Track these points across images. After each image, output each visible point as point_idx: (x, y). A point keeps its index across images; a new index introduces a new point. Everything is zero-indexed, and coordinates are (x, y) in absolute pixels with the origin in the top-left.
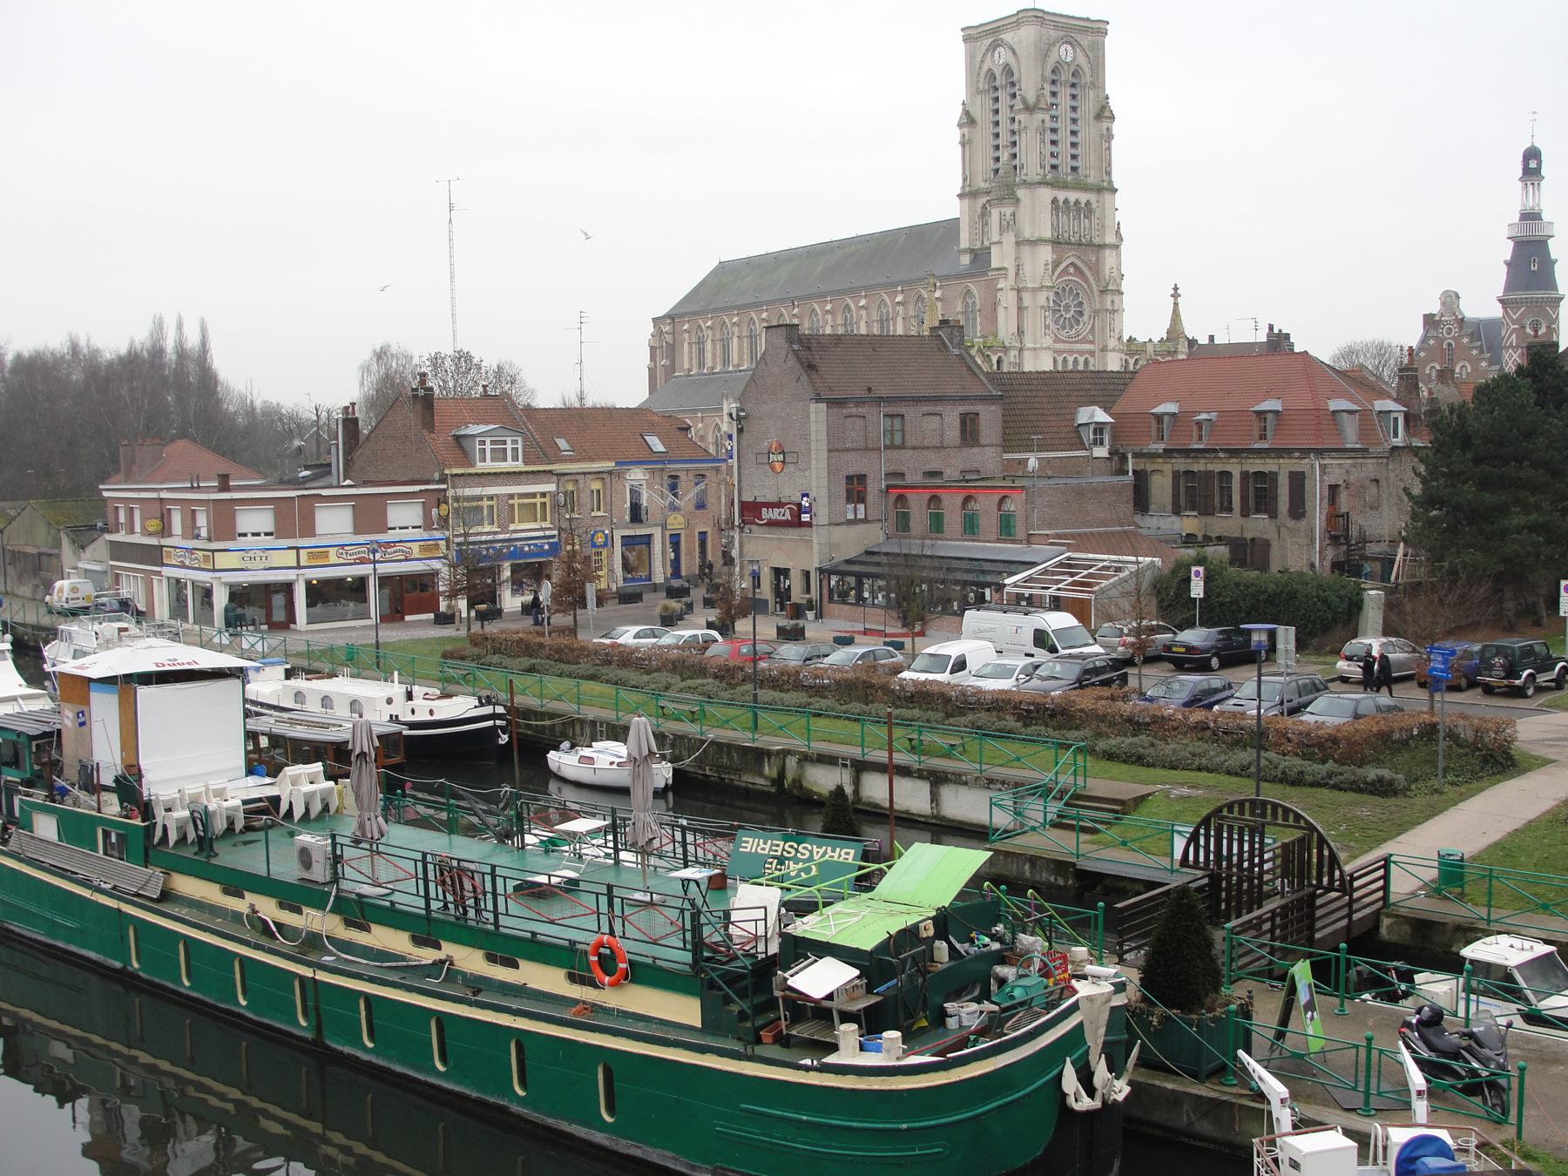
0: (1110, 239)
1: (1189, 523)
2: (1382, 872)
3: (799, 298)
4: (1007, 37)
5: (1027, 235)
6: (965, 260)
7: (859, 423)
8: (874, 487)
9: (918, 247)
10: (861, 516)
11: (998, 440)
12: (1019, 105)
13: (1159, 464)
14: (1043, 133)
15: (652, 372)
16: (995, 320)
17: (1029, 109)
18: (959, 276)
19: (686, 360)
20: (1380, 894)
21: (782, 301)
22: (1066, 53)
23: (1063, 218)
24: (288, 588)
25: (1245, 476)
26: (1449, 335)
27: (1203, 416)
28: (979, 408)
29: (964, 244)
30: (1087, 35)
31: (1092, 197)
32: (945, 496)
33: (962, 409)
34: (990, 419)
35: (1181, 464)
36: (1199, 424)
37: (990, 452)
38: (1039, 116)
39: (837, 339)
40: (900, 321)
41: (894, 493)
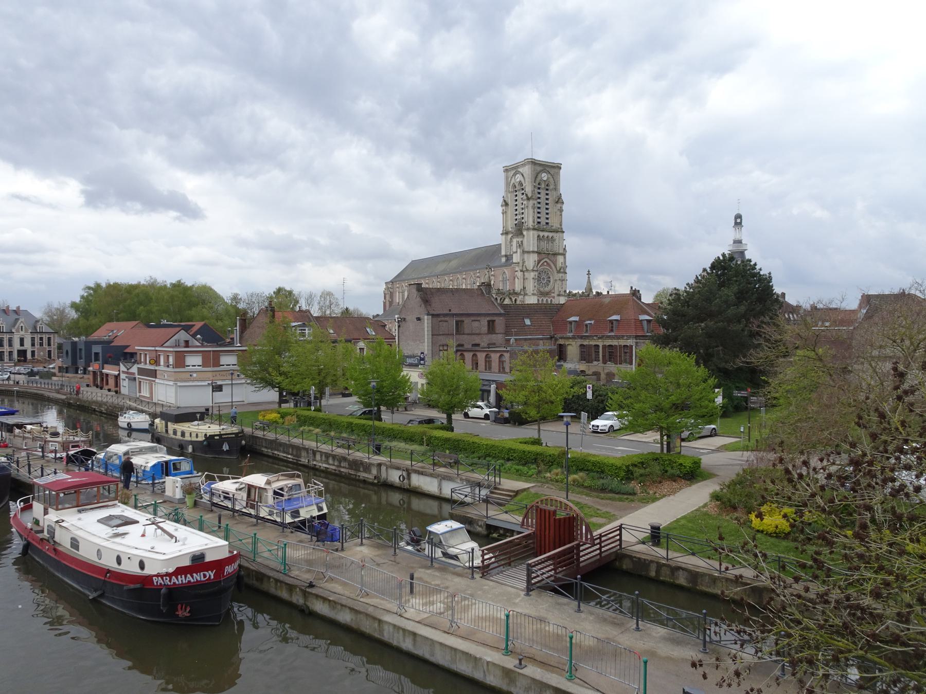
1: (582, 366)
2: (618, 532)
4: (520, 170)
5: (526, 250)
6: (504, 260)
7: (445, 324)
9: (486, 257)
11: (503, 331)
13: (570, 342)
14: (534, 208)
15: (385, 303)
16: (514, 284)
17: (528, 199)
18: (501, 266)
20: (618, 537)
21: (434, 276)
22: (544, 176)
23: (542, 243)
25: (604, 347)
28: (464, 319)
29: (503, 253)
30: (553, 169)
32: (479, 354)
33: (488, 319)
34: (500, 323)
35: (580, 342)
38: (531, 202)
41: (459, 353)
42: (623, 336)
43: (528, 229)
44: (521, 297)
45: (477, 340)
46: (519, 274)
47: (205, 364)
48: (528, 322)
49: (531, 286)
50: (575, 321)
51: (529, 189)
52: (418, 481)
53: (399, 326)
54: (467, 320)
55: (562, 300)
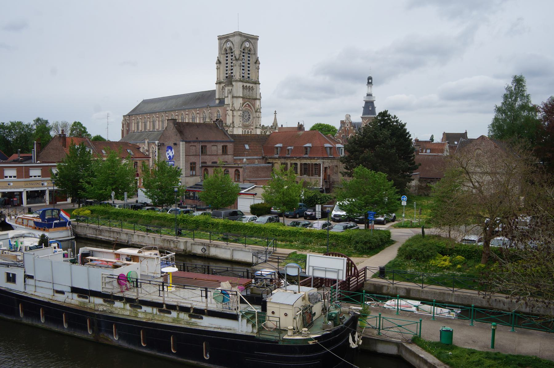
0: (258, 97)
3: (168, 111)
4: (231, 39)
6: (217, 102)
7: (194, 148)
8: (198, 166)
9: (202, 99)
10: (194, 173)
12: (234, 59)
13: (277, 161)
15: (123, 131)
17: (237, 60)
19: (133, 127)
21: (163, 112)
22: (247, 45)
23: (245, 91)
24: (21, 193)
26: (347, 127)
27: (289, 148)
28: (227, 144)
29: (217, 97)
30: (252, 39)
31: (253, 85)
33: (222, 144)
34: (230, 146)
36: (288, 150)
37: (230, 157)
39: (188, 124)
40: (198, 119)
41: (204, 168)
42: (314, 158)
43: (236, 81)
44: (231, 128)
45: (215, 159)
46: (230, 113)
47: (19, 176)
48: (247, 147)
49: (238, 121)
50: (280, 147)
51: (237, 53)
52: (213, 252)
53: (159, 149)
54: (209, 145)
55: (259, 132)
